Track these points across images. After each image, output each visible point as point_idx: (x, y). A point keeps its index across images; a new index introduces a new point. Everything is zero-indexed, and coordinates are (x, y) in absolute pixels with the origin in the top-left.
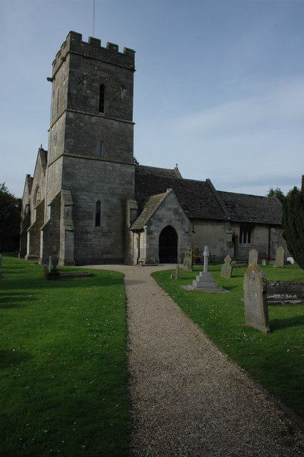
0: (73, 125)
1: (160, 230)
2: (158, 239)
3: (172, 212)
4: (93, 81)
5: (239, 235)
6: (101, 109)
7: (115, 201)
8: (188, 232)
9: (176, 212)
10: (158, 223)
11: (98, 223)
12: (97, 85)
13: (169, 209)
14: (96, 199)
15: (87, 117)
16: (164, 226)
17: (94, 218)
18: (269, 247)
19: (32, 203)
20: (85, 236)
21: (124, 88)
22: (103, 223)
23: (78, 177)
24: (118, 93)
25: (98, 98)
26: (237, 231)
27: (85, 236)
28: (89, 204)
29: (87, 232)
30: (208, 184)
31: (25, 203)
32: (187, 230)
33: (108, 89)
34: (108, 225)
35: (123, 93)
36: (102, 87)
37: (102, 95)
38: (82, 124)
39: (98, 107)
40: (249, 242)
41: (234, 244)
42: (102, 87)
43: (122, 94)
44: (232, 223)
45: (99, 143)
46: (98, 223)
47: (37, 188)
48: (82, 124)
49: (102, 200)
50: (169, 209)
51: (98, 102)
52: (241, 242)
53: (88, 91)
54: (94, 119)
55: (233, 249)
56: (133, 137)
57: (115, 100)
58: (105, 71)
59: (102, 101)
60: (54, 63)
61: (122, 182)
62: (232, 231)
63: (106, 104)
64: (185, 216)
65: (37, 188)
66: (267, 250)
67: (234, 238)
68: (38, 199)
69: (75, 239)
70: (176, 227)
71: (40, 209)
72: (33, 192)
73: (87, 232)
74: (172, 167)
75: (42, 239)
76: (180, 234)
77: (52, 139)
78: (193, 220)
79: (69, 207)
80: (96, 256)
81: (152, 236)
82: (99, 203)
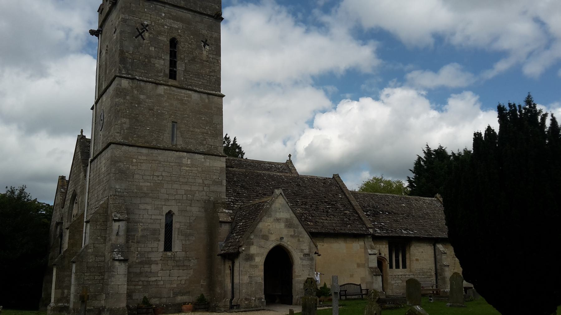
0: (128, 97)
1: (265, 252)
2: (262, 267)
3: (282, 225)
4: (159, 33)
5: (387, 257)
6: (173, 75)
7: (196, 210)
8: (308, 255)
9: (289, 224)
10: (262, 242)
11: (168, 247)
12: (165, 39)
13: (278, 220)
14: (166, 210)
15: (150, 86)
16: (271, 247)
17: (162, 237)
18: (436, 274)
19: (65, 220)
20: (146, 269)
21: (206, 44)
22: (177, 246)
23: (136, 176)
24: (197, 52)
25: (168, 58)
26: (384, 249)
27: (146, 269)
28: (153, 217)
29: (149, 262)
30: (496, 309)
31: (56, 219)
32: (306, 251)
33: (183, 46)
34: (185, 249)
35: (218, 67)
36: (173, 43)
37: (173, 55)
38: (142, 97)
39: (167, 72)
40: (404, 266)
41: (381, 270)
42: (173, 43)
43: (205, 53)
44: (376, 239)
45: (170, 125)
46: (168, 247)
47: (74, 196)
48: (142, 97)
49: (175, 210)
50: (278, 220)
51: (168, 63)
52: (391, 267)
53: (152, 49)
54: (161, 90)
55: (380, 278)
56: (222, 115)
57: (193, 60)
58: (176, 19)
59: (173, 63)
60: (101, 10)
61: (206, 182)
62: (376, 251)
63: (180, 68)
64: (301, 229)
65: (74, 196)
66: (434, 278)
67: (380, 262)
68: (75, 212)
69: (129, 273)
70: (290, 247)
71: (76, 229)
72: (68, 203)
73: (149, 262)
74: (283, 159)
75: (73, 276)
76: (297, 257)
77: (98, 120)
78: (315, 236)
79: (121, 224)
80: (164, 300)
81: (253, 263)
82: (170, 214)
